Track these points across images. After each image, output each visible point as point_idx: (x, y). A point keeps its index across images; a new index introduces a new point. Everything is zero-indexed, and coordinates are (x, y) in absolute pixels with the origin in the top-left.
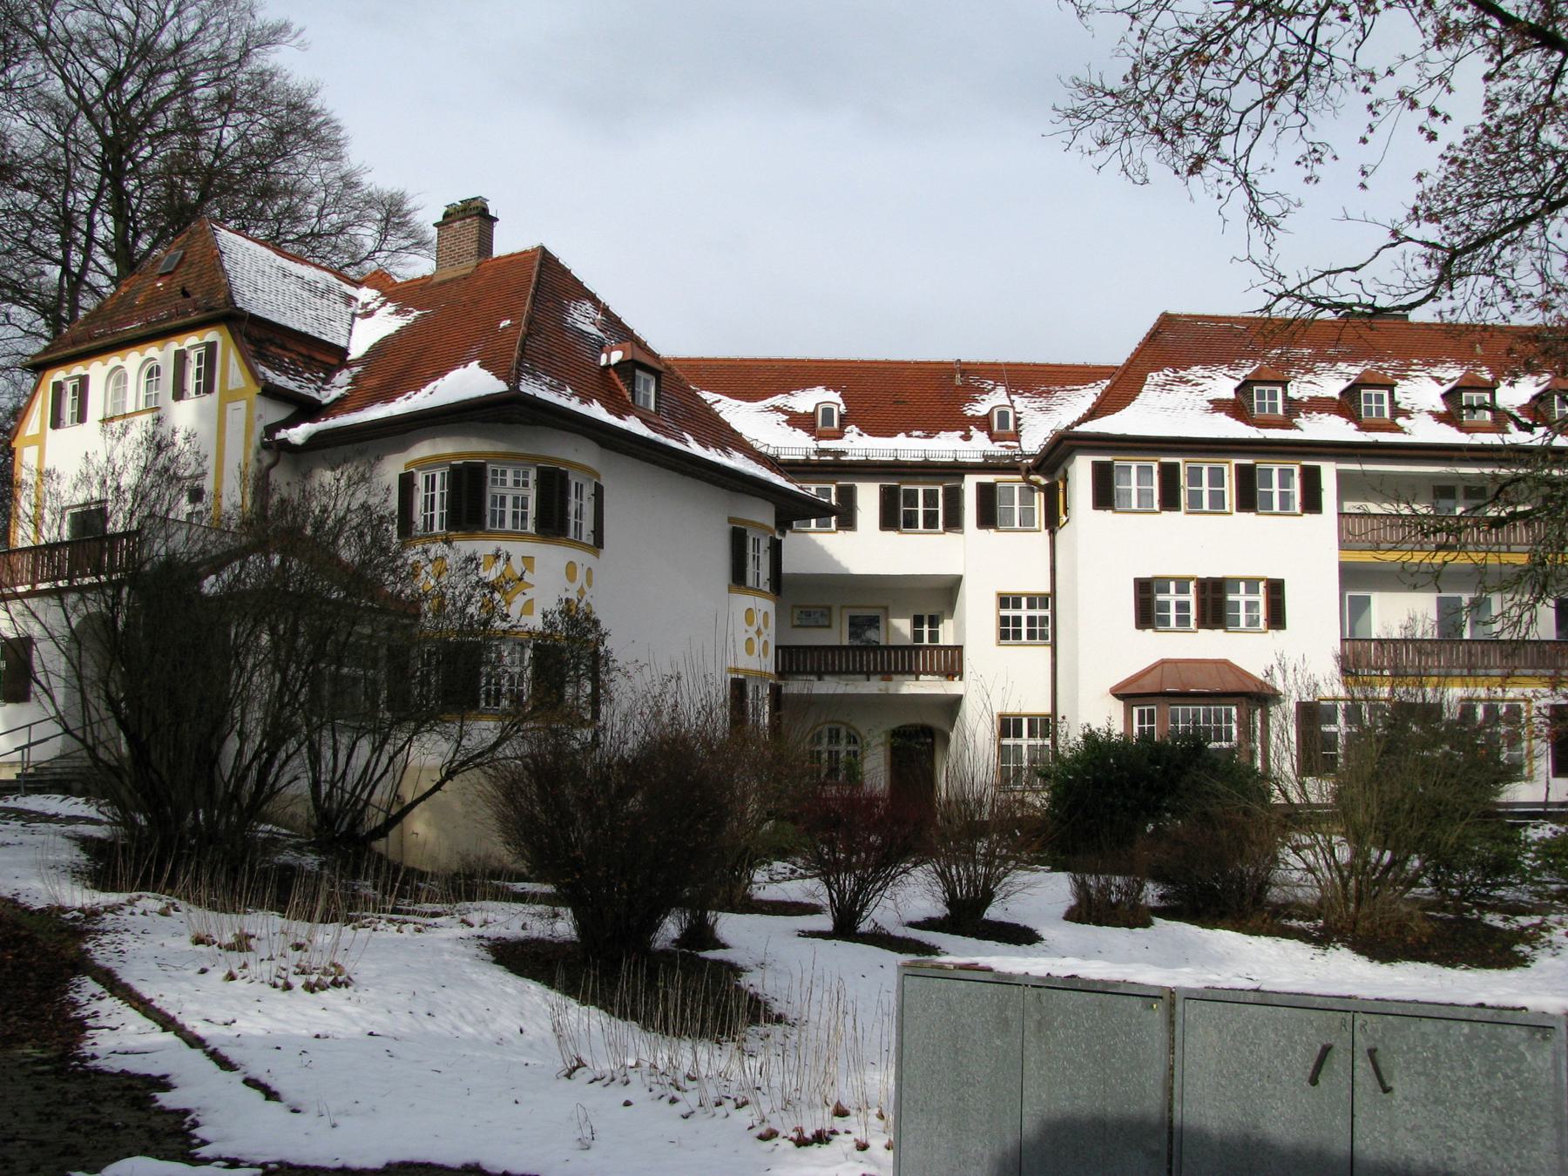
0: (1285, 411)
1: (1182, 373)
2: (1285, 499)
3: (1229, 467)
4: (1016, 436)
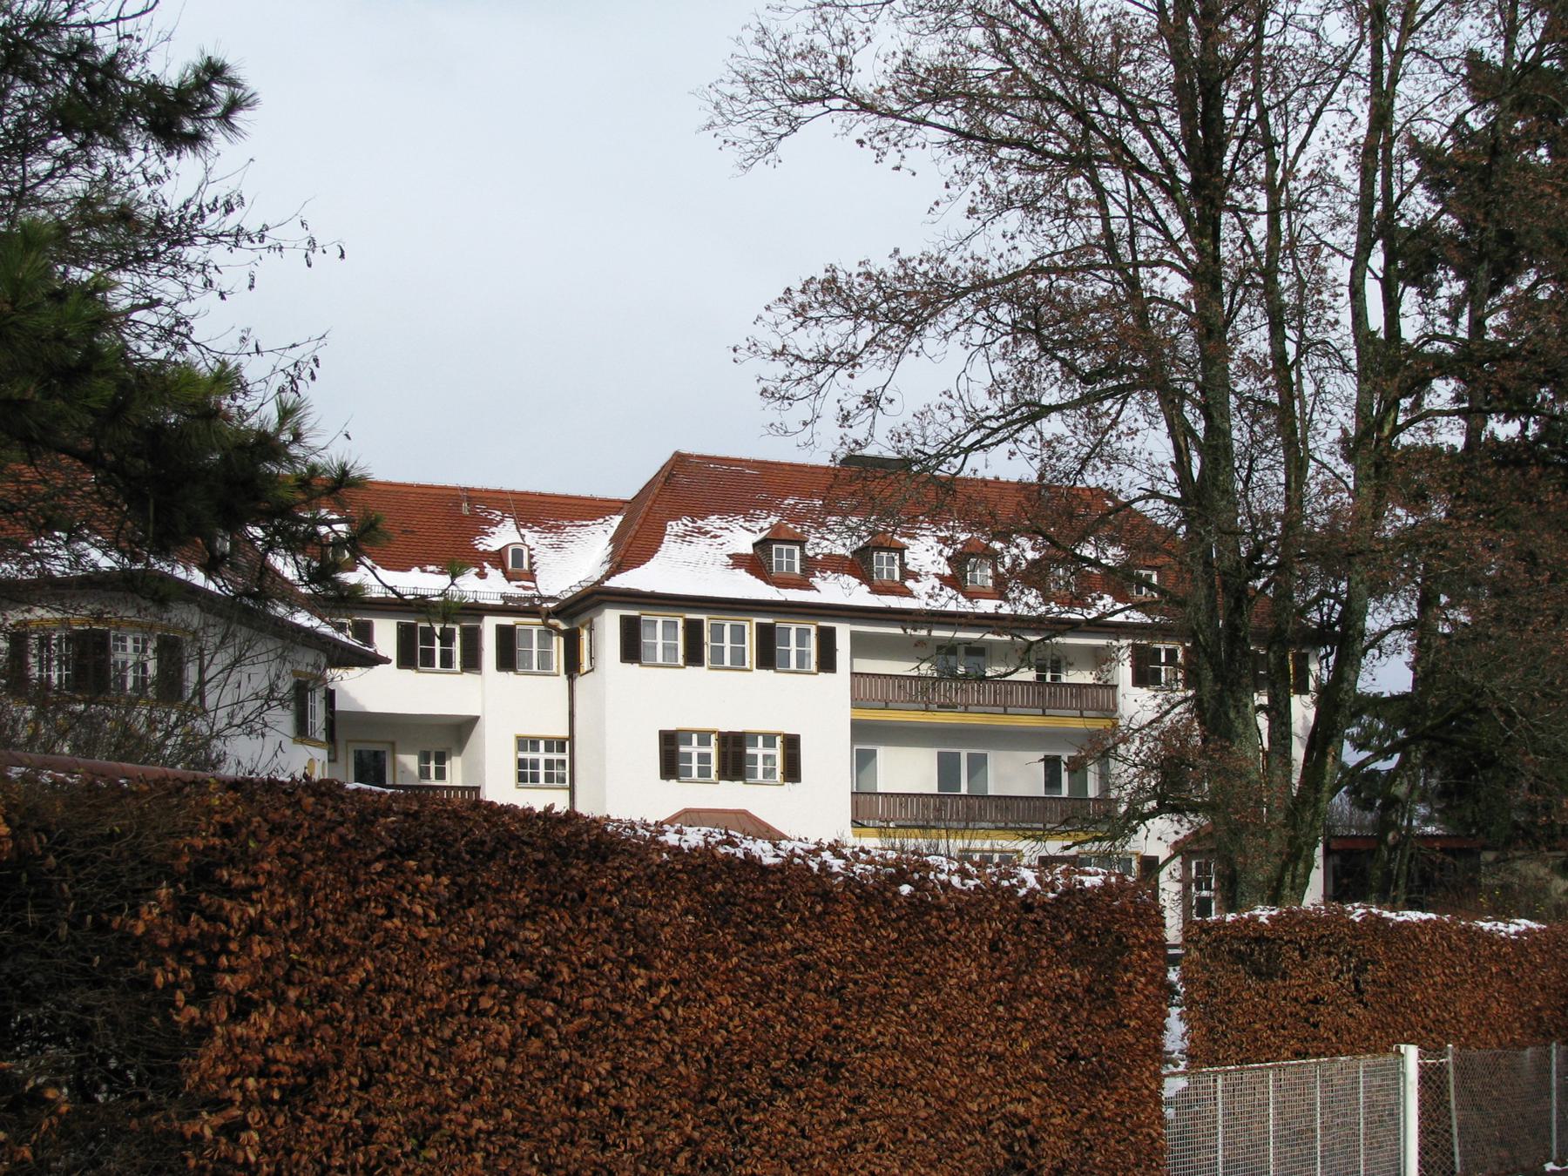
0: (802, 570)
1: (700, 523)
2: (802, 658)
3: (750, 626)
4: (531, 575)
